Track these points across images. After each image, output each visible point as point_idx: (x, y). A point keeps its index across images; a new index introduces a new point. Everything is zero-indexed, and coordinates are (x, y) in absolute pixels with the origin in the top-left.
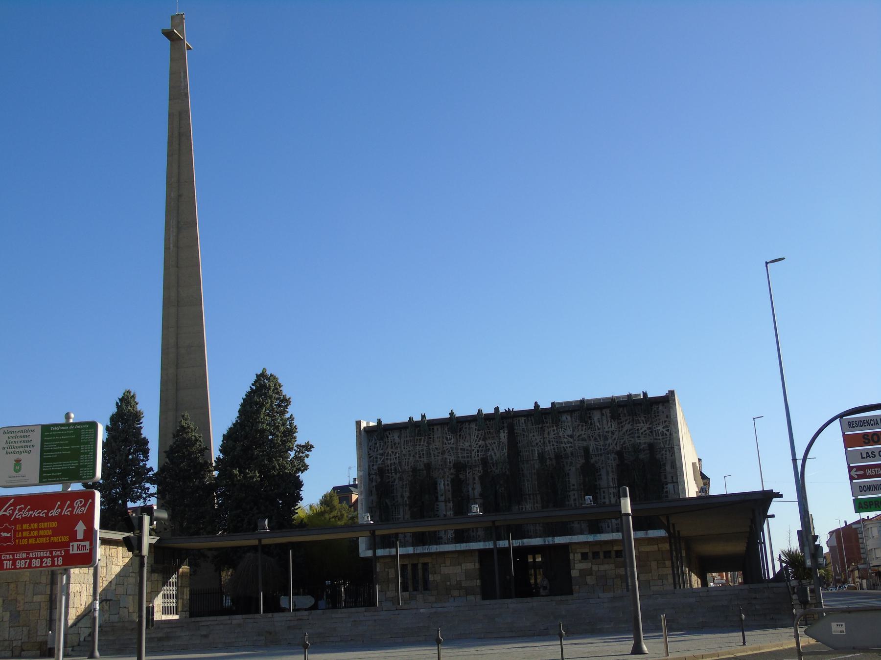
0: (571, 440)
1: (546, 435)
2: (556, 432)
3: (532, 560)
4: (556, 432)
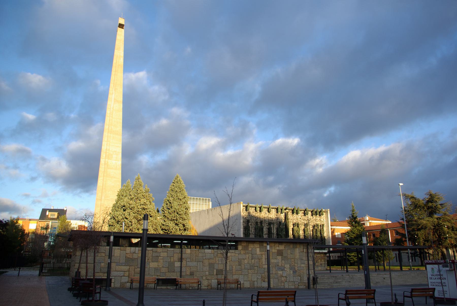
0: (300, 220)
1: (294, 217)
2: (296, 216)
3: (345, 267)
4: (296, 216)
